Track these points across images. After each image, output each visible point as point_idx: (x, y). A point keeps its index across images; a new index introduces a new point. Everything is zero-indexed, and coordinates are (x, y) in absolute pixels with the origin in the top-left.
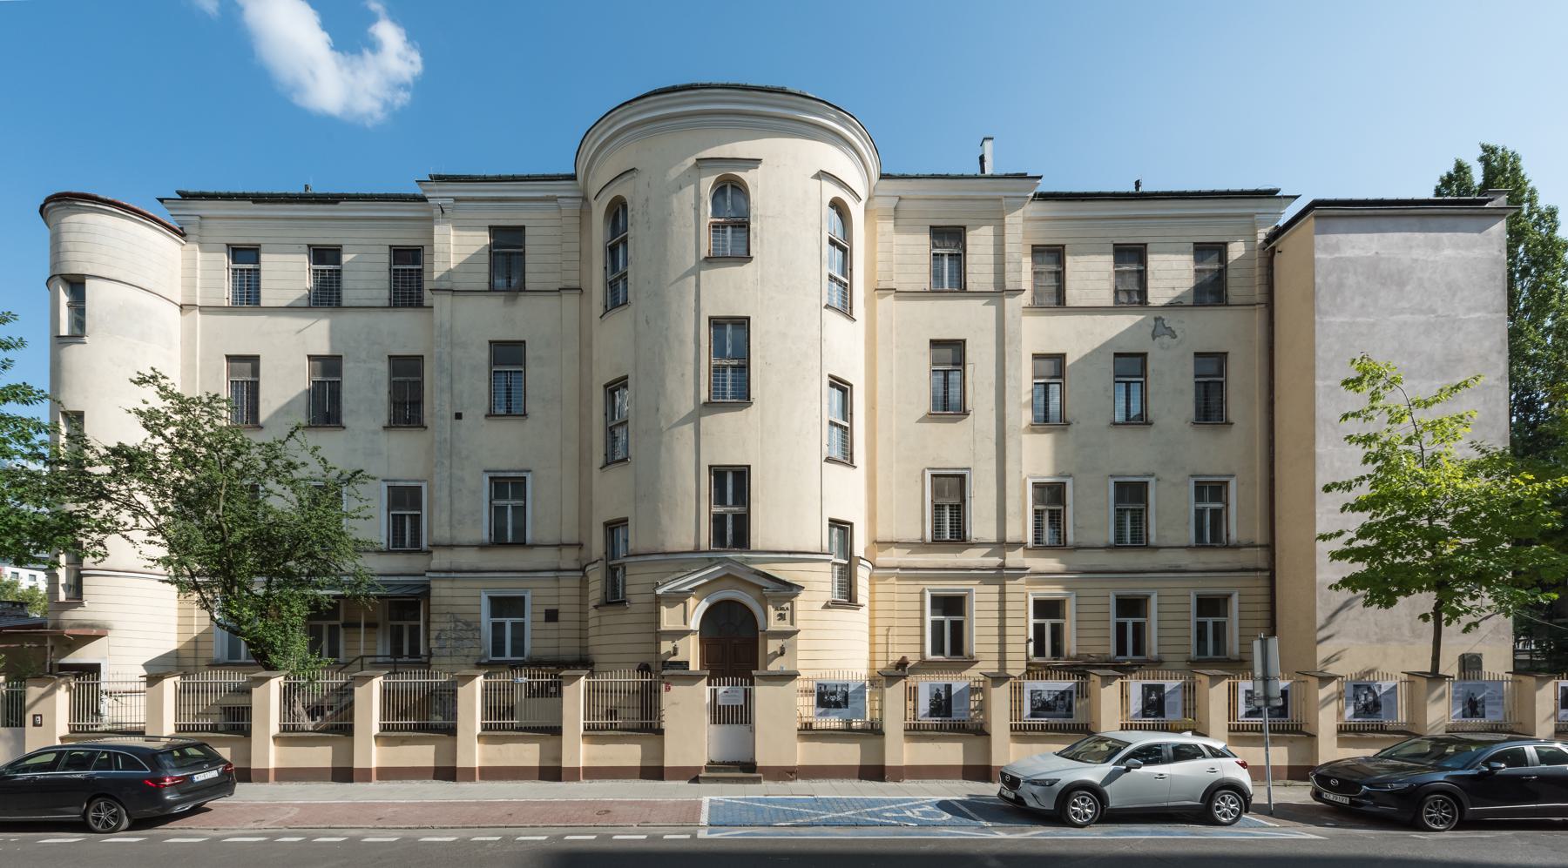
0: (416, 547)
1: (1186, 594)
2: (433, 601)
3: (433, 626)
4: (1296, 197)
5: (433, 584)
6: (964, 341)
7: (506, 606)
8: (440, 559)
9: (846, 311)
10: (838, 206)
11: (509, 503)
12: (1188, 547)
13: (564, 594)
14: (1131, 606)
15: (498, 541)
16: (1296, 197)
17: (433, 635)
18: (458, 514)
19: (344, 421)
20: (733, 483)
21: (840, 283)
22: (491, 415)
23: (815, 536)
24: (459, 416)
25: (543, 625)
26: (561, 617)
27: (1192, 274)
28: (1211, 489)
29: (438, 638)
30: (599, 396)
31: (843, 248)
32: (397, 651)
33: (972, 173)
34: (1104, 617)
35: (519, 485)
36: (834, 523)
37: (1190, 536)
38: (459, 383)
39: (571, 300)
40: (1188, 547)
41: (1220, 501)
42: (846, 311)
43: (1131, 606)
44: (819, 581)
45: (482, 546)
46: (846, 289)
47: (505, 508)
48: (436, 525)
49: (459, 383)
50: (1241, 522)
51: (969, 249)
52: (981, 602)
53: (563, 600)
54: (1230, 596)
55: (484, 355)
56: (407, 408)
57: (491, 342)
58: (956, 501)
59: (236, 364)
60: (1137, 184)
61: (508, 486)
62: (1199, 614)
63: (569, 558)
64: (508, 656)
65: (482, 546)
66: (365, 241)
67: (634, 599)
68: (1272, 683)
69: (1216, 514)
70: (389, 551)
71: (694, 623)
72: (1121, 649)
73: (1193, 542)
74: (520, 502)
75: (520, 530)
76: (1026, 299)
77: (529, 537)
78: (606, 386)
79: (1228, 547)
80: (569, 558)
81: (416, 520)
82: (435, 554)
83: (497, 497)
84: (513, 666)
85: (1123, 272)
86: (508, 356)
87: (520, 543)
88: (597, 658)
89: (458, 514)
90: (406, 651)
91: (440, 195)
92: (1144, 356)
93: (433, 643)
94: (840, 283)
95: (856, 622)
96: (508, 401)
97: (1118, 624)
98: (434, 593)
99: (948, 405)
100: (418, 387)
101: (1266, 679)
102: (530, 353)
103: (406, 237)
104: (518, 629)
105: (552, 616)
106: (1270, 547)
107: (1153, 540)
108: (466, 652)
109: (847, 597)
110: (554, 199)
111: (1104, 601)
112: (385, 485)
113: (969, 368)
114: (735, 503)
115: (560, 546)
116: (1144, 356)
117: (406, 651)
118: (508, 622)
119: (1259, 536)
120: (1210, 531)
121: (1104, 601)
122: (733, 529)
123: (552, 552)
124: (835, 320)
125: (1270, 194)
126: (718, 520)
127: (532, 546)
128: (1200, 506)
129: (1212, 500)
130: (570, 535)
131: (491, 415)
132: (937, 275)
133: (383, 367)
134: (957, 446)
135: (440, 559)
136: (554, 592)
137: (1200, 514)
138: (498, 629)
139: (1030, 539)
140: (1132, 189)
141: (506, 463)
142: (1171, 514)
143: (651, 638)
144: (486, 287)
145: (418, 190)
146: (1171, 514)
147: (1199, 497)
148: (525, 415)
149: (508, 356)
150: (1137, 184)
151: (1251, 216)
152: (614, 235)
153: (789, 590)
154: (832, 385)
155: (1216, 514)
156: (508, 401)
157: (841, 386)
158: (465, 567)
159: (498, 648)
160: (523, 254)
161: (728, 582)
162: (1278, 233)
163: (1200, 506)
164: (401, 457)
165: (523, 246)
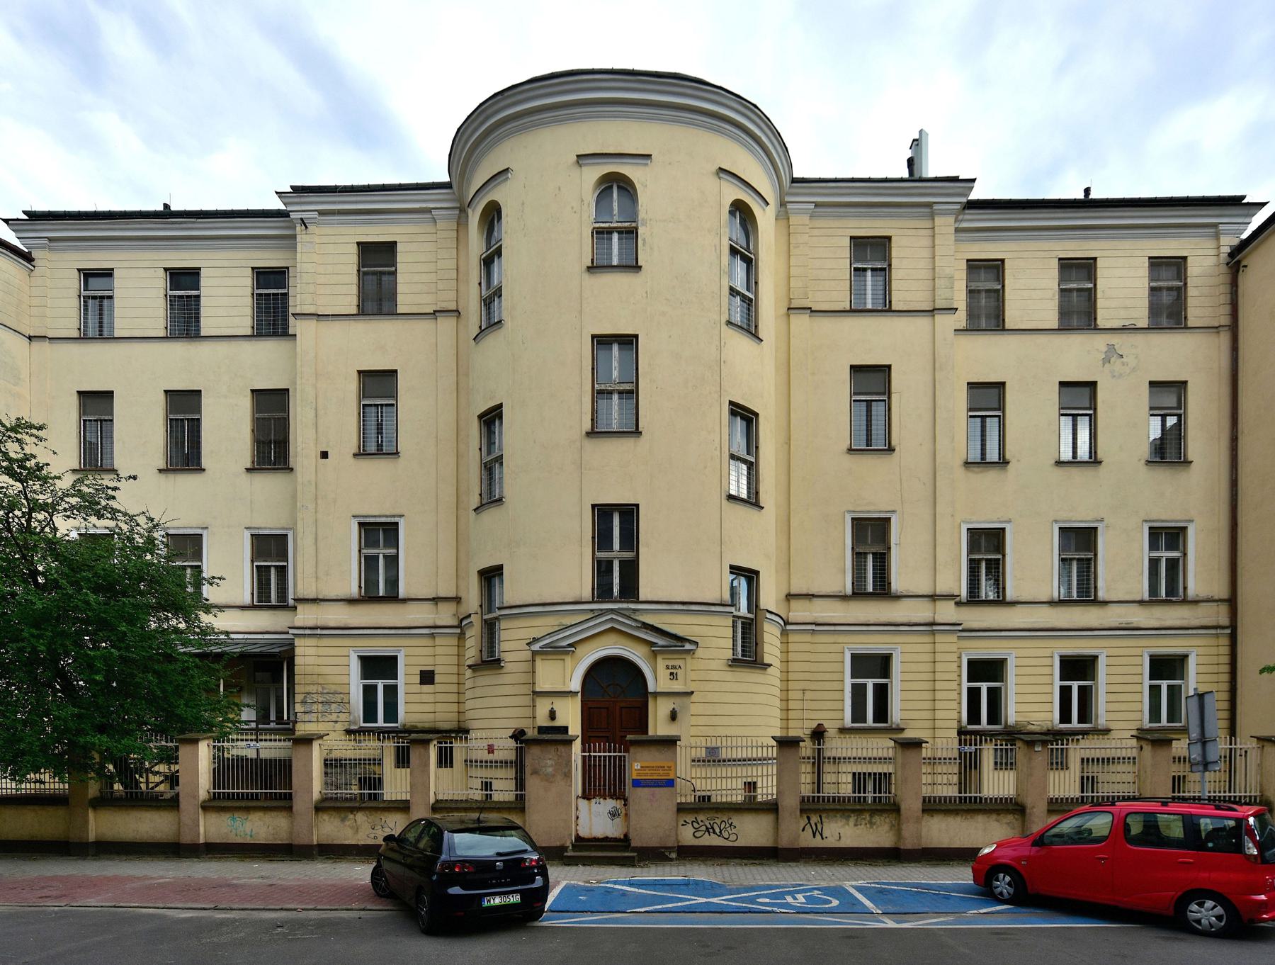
0: (284, 604)
1: (1139, 655)
2: (298, 660)
3: (297, 689)
4: (1263, 204)
5: (297, 642)
6: (889, 367)
7: (379, 666)
8: (305, 616)
9: (750, 329)
10: (741, 211)
11: (382, 552)
12: (1141, 602)
13: (441, 656)
14: (1078, 667)
15: (369, 597)
16: (1263, 204)
17: (298, 698)
18: (327, 563)
19: (205, 462)
20: (616, 524)
21: (744, 298)
22: (361, 454)
23: (716, 585)
24: (325, 455)
25: (418, 688)
26: (437, 678)
27: (1147, 293)
28: (1168, 537)
29: (304, 702)
30: (474, 429)
31: (745, 255)
32: (263, 717)
33: (899, 176)
34: (1046, 679)
35: (391, 530)
36: (736, 570)
37: (1142, 589)
38: (326, 417)
39: (446, 324)
40: (1141, 602)
41: (1175, 548)
42: (750, 329)
43: (1078, 667)
44: (717, 638)
45: (351, 601)
46: (750, 304)
47: (377, 557)
48: (302, 581)
49: (326, 417)
50: (1202, 575)
51: (894, 263)
52: (908, 661)
53: (439, 660)
54: (1187, 656)
55: (353, 385)
56: (272, 450)
57: (359, 372)
58: (879, 549)
59: (861, 376)
60: (1087, 191)
61: (379, 534)
62: (365, 676)
63: (445, 615)
64: (381, 723)
65: (351, 601)
66: (226, 264)
67: (507, 657)
68: (1210, 746)
69: (1173, 565)
70: (252, 607)
71: (575, 684)
72: (1065, 716)
73: (1146, 597)
74: (393, 551)
75: (393, 582)
76: (961, 319)
77: (402, 592)
78: (480, 417)
79: (1185, 601)
80: (445, 615)
81: (282, 571)
82: (300, 607)
83: (367, 546)
84: (381, 734)
85: (1070, 290)
86: (378, 385)
87: (393, 597)
88: (472, 725)
89: (327, 563)
90: (273, 717)
91: (299, 210)
92: (1093, 385)
93: (298, 708)
94: (744, 298)
95: (763, 689)
96: (377, 442)
97: (1061, 688)
98: (298, 651)
99: (873, 439)
100: (283, 425)
101: (1204, 741)
102: (402, 382)
103: (270, 259)
104: (391, 692)
105: (427, 678)
106: (1232, 602)
107: (1102, 595)
108: (334, 717)
109: (748, 656)
110: (429, 211)
111: (1048, 661)
112: (247, 534)
113: (894, 397)
114: (622, 547)
115: (436, 600)
116: (1093, 385)
117: (273, 717)
118: (380, 684)
119: (1221, 591)
120: (1167, 583)
121: (1048, 661)
122: (617, 577)
123: (428, 606)
124: (740, 342)
125: (1235, 202)
126: (602, 569)
127: (405, 601)
128: (1155, 554)
129: (1168, 548)
130: (446, 590)
131: (361, 454)
132: (856, 290)
133: (246, 403)
134: (874, 486)
135: (305, 616)
136: (429, 651)
137: (1154, 563)
138: (369, 692)
139: (964, 593)
140: (1081, 196)
141: (377, 509)
142: (1123, 566)
143: (527, 700)
144: (354, 311)
145: (278, 205)
146: (1123, 566)
147: (1154, 546)
148: (397, 453)
149: (378, 385)
150: (1087, 191)
151: (1215, 225)
152: (488, 246)
153: (678, 644)
154: (733, 413)
155: (1173, 565)
156: (377, 442)
157: (744, 415)
158: (332, 624)
159: (370, 713)
160: (394, 273)
161: (612, 638)
162: (1245, 244)
163: (1155, 554)
164: (264, 503)
165: (394, 264)
